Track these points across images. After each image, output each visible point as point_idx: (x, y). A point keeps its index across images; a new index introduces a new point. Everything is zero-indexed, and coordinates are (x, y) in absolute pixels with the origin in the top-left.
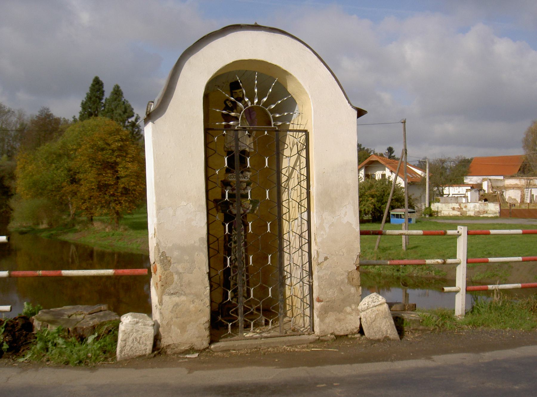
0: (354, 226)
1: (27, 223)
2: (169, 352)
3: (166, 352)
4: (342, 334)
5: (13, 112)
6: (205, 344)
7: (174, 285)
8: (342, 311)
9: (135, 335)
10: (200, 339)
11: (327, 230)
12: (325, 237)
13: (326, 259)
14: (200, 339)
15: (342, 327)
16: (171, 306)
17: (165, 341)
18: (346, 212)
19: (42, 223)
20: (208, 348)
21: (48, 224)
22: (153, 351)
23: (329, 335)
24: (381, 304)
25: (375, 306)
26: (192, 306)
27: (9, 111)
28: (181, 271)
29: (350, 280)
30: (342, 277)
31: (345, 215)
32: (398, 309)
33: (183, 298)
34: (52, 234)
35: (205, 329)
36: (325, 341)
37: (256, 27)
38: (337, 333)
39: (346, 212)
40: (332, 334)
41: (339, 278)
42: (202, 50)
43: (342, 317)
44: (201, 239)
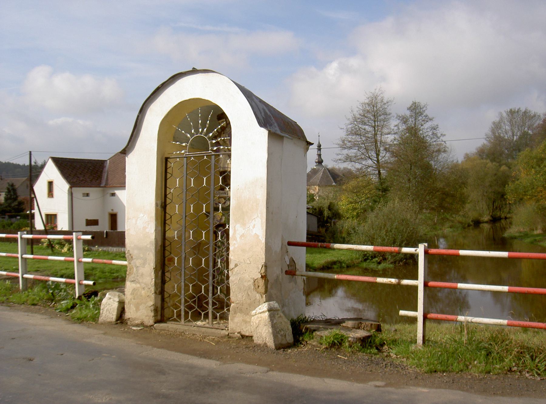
0: (260, 238)
1: (524, 229)
2: (129, 323)
3: (127, 323)
4: (247, 334)
5: (539, 116)
6: (151, 322)
7: (133, 275)
8: (248, 314)
9: (108, 306)
10: (148, 318)
11: (238, 239)
12: (236, 246)
13: (236, 265)
14: (148, 318)
15: (247, 329)
16: (131, 290)
17: (128, 315)
18: (254, 225)
19: (536, 229)
20: (153, 325)
21: (543, 230)
22: (117, 320)
23: (236, 334)
24: (263, 312)
25: (261, 313)
26: (143, 292)
27: (535, 116)
28: (138, 265)
29: (256, 287)
30: (249, 284)
31: (254, 227)
32: (349, 326)
33: (138, 285)
34: (535, 240)
35: (151, 311)
36: (233, 338)
37: (194, 71)
38: (243, 333)
39: (254, 225)
40: (238, 333)
41: (246, 284)
42: (159, 98)
43: (248, 320)
44: (151, 242)
